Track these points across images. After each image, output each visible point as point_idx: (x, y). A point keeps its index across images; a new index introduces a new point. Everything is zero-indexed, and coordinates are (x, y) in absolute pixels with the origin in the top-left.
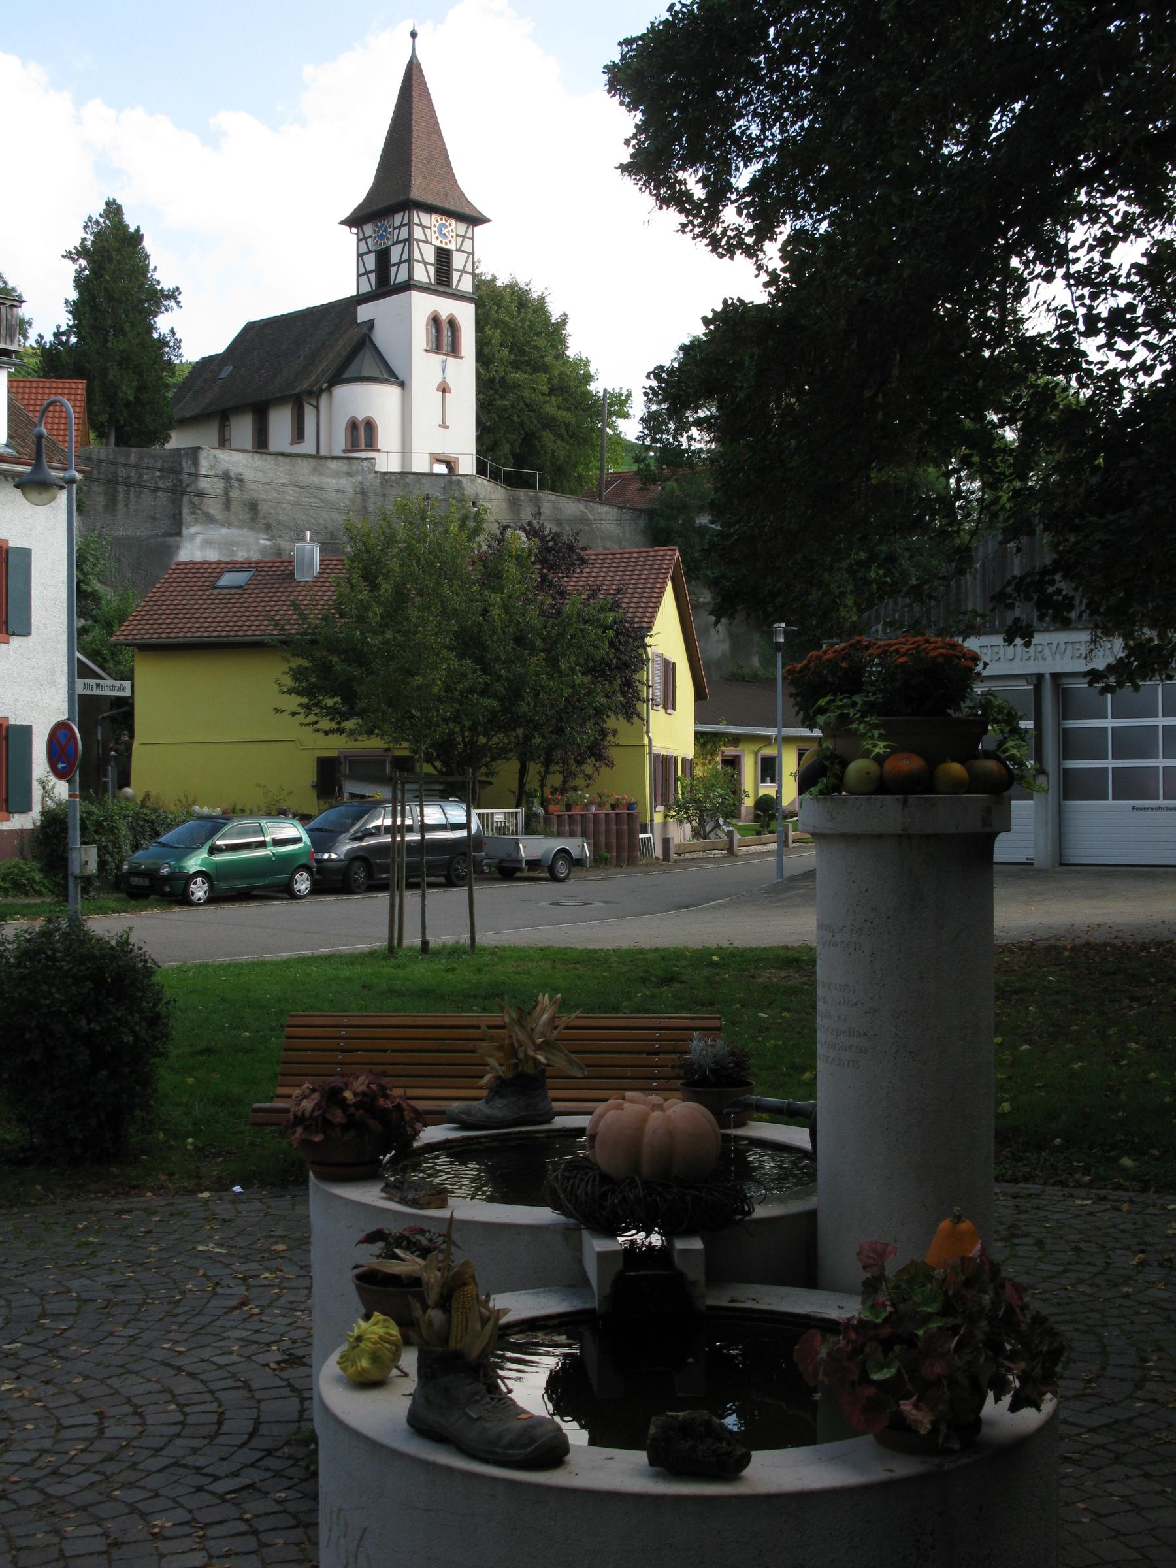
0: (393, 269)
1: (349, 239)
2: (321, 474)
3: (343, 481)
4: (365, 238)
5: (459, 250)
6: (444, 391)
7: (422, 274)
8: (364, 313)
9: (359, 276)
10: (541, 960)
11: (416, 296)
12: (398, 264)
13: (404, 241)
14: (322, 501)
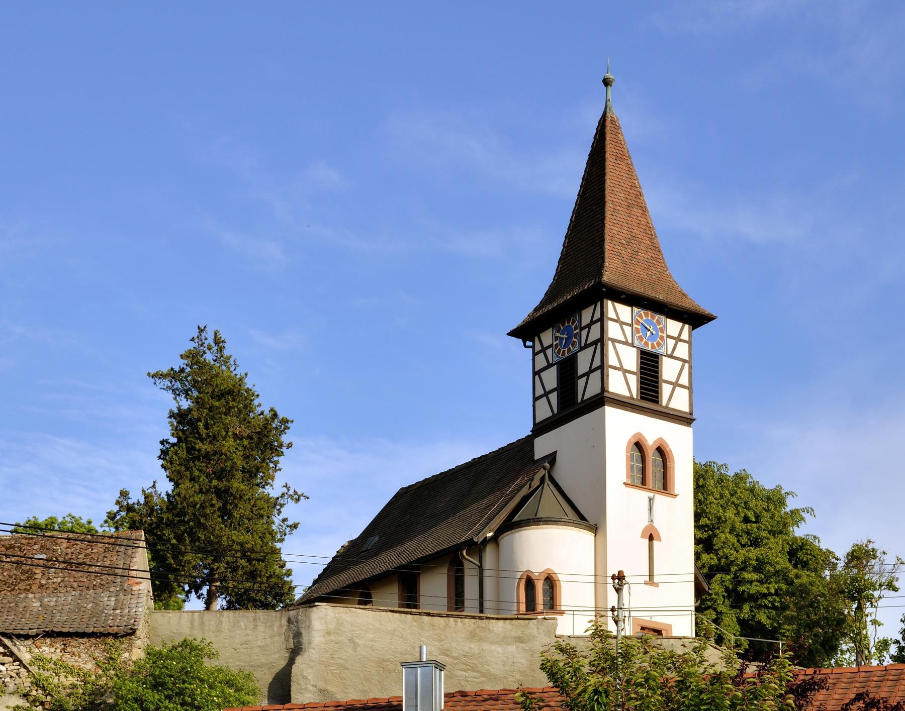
0: (581, 383)
1: (520, 355)
2: (481, 640)
3: (512, 649)
4: (544, 350)
5: (671, 356)
6: (651, 538)
7: (622, 382)
8: (542, 447)
9: (535, 399)
10: (265, 557)
11: (611, 412)
12: (587, 374)
13: (595, 343)
14: (483, 675)
